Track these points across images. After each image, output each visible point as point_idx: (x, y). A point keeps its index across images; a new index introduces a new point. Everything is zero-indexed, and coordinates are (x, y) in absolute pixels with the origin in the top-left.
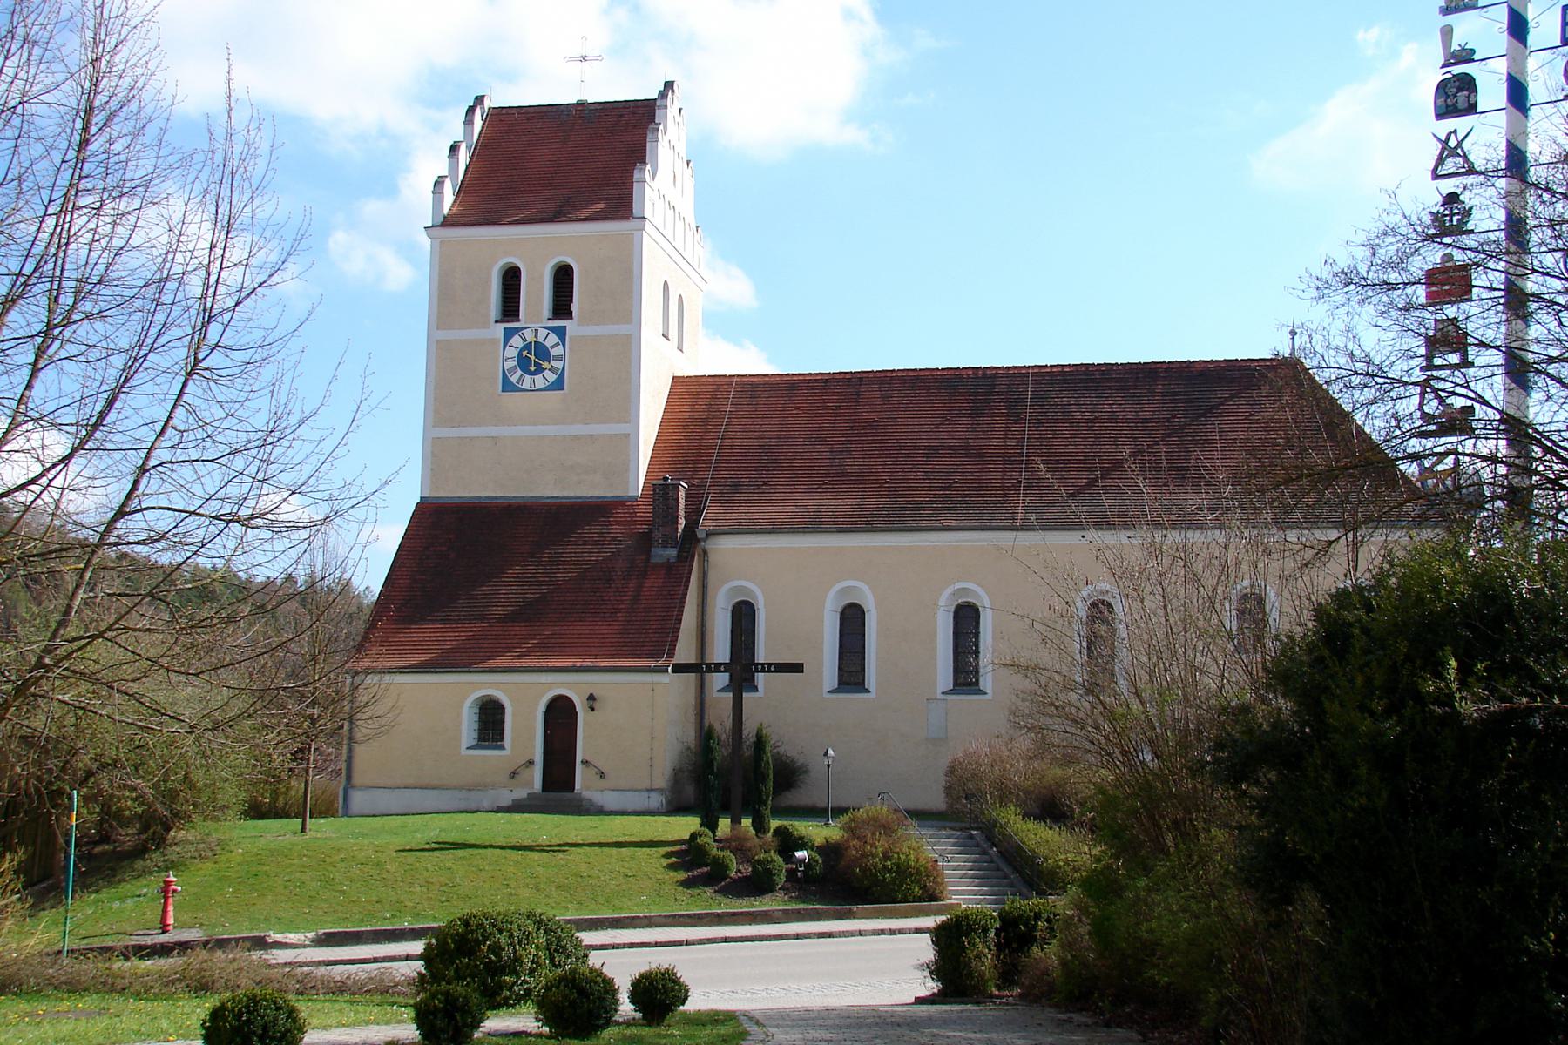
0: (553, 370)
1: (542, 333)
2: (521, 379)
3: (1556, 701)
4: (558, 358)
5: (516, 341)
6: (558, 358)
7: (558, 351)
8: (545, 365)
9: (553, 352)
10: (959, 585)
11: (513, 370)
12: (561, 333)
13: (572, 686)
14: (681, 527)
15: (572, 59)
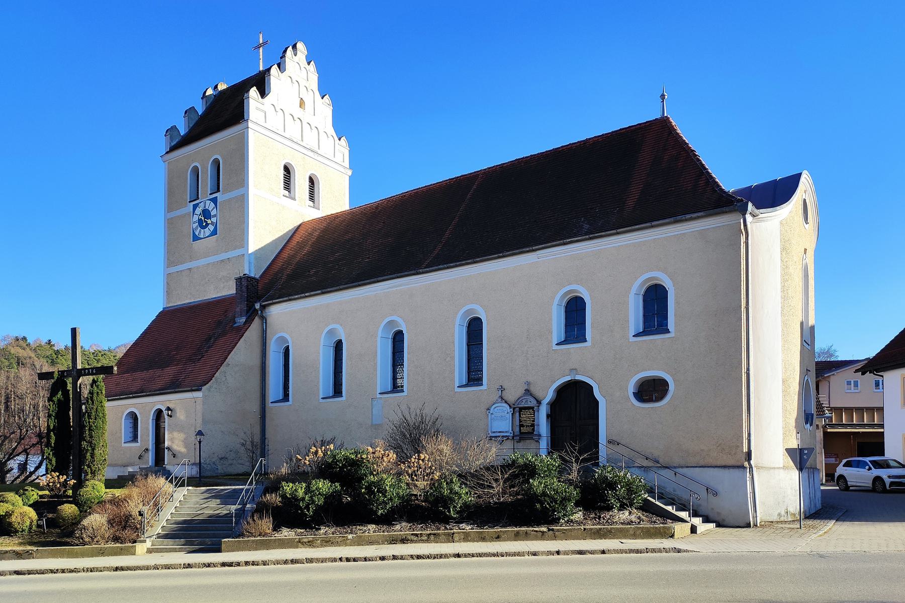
0: (212, 223)
4: (215, 216)
6: (215, 216)
8: (209, 221)
10: (325, 331)
12: (214, 200)
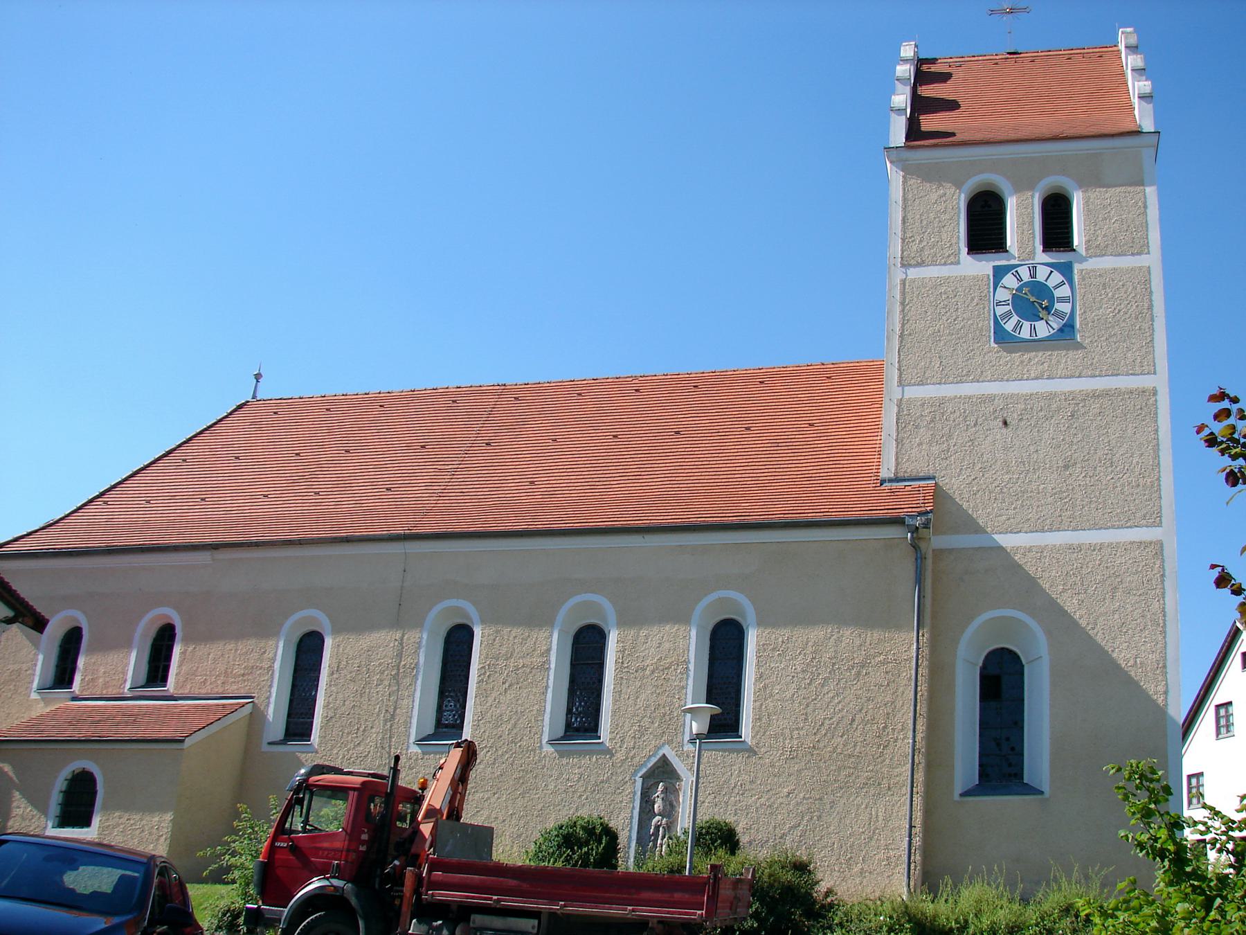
1: (1002, 295)
2: (1018, 326)
3: (397, 862)
5: (1009, 281)
7: (1065, 291)
9: (1058, 293)
11: (1008, 315)
13: (265, 742)
14: (11, 774)
15: (1025, 10)
